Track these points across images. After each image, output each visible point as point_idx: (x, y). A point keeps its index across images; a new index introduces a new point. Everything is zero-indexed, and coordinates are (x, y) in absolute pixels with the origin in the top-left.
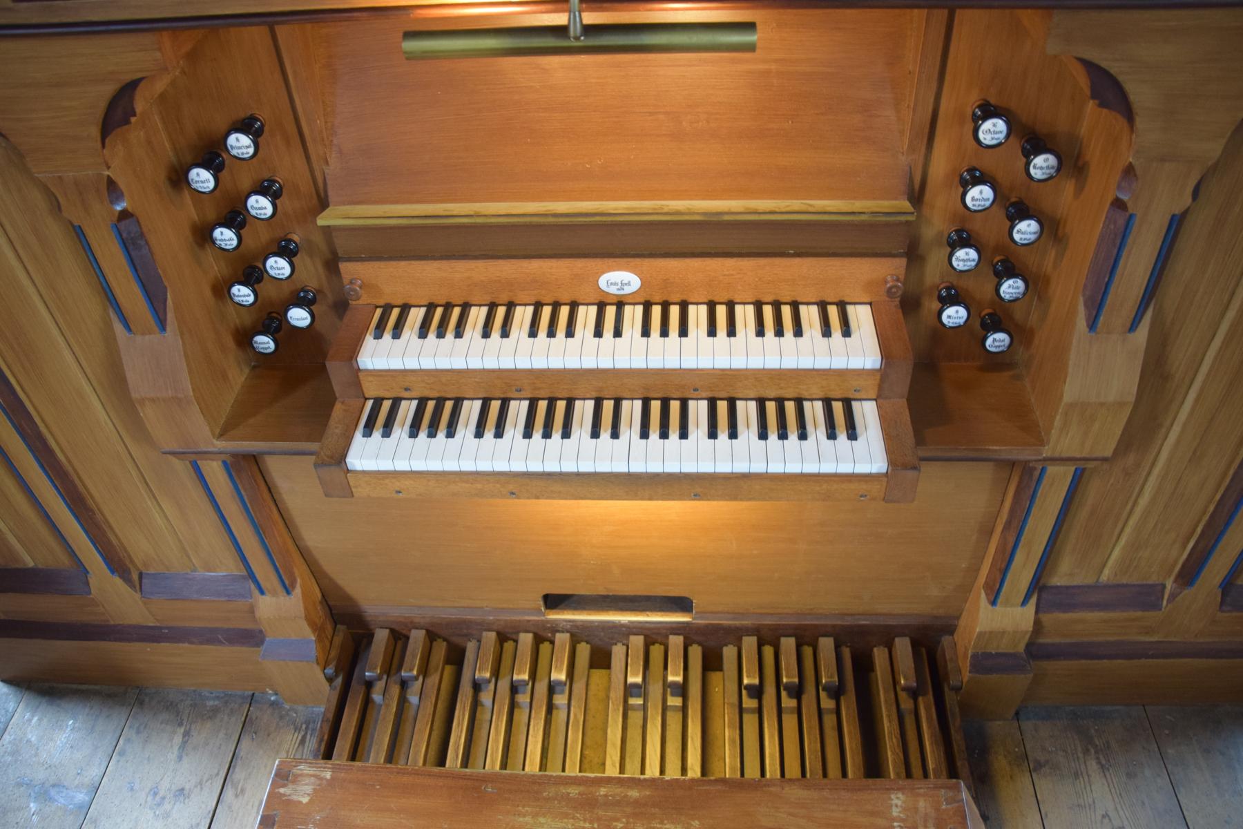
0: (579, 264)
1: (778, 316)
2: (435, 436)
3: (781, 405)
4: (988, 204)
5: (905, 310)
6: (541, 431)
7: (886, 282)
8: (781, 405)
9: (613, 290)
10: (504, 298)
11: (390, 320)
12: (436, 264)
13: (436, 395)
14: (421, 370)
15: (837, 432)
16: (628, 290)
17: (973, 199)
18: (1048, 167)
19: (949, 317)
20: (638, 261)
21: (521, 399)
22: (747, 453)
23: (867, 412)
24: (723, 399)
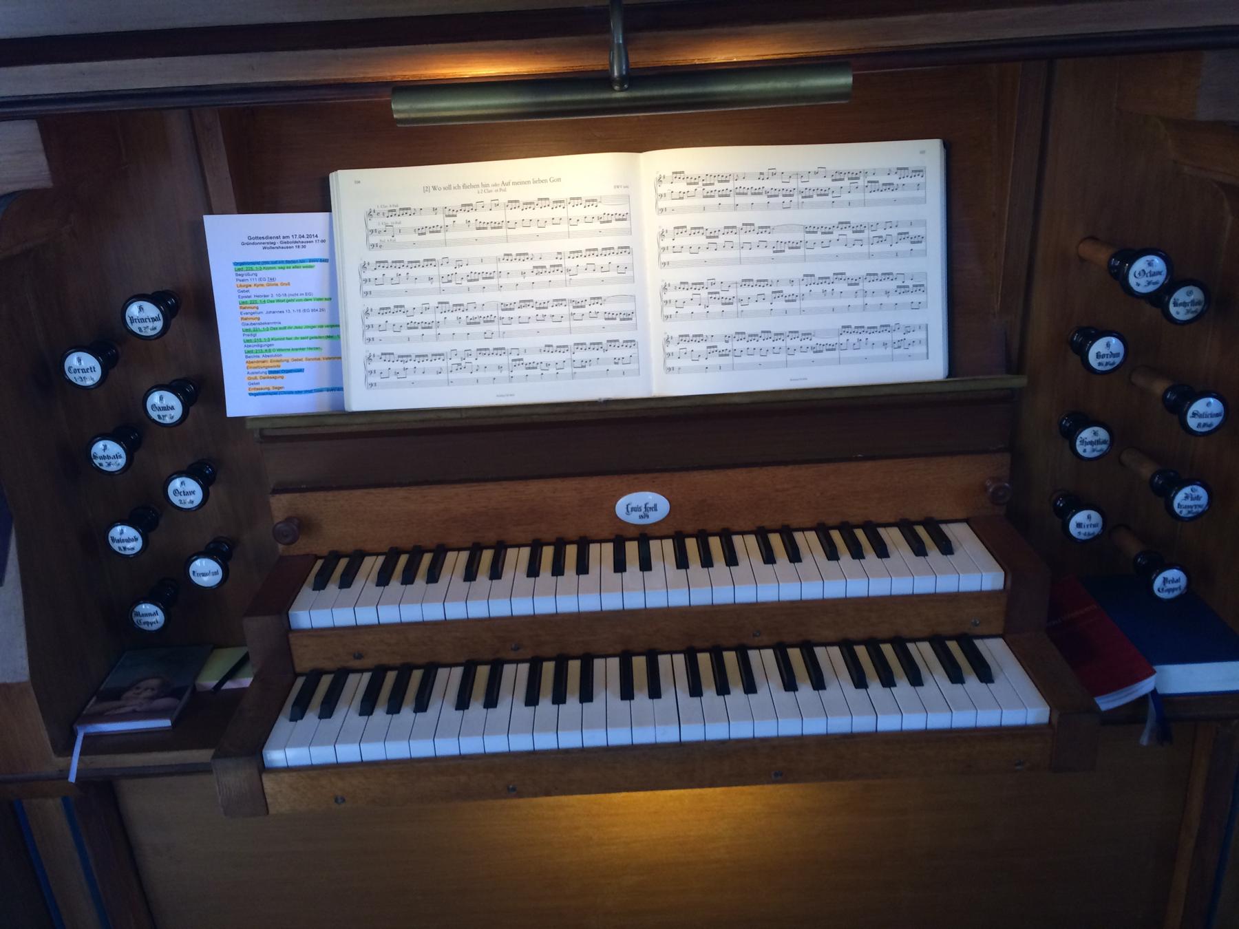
0: (591, 485)
1: (853, 536)
2: (398, 712)
3: (877, 642)
4: (1118, 360)
5: (1014, 528)
6: (550, 697)
7: (986, 489)
8: (877, 642)
9: (634, 519)
10: (491, 537)
11: (338, 568)
12: (401, 492)
13: (398, 661)
14: (379, 625)
15: (965, 675)
16: (654, 517)
17: (1098, 355)
18: (1193, 303)
19: (1079, 525)
20: (666, 476)
21: (517, 662)
22: (839, 709)
23: (994, 650)
24: (795, 640)
